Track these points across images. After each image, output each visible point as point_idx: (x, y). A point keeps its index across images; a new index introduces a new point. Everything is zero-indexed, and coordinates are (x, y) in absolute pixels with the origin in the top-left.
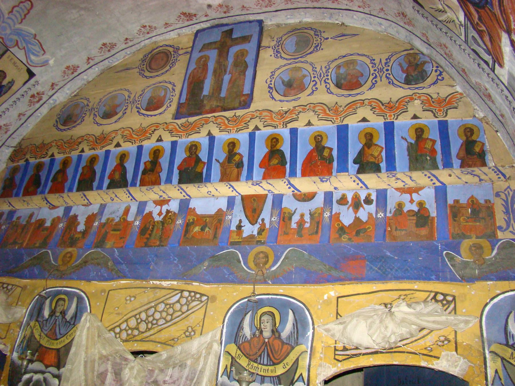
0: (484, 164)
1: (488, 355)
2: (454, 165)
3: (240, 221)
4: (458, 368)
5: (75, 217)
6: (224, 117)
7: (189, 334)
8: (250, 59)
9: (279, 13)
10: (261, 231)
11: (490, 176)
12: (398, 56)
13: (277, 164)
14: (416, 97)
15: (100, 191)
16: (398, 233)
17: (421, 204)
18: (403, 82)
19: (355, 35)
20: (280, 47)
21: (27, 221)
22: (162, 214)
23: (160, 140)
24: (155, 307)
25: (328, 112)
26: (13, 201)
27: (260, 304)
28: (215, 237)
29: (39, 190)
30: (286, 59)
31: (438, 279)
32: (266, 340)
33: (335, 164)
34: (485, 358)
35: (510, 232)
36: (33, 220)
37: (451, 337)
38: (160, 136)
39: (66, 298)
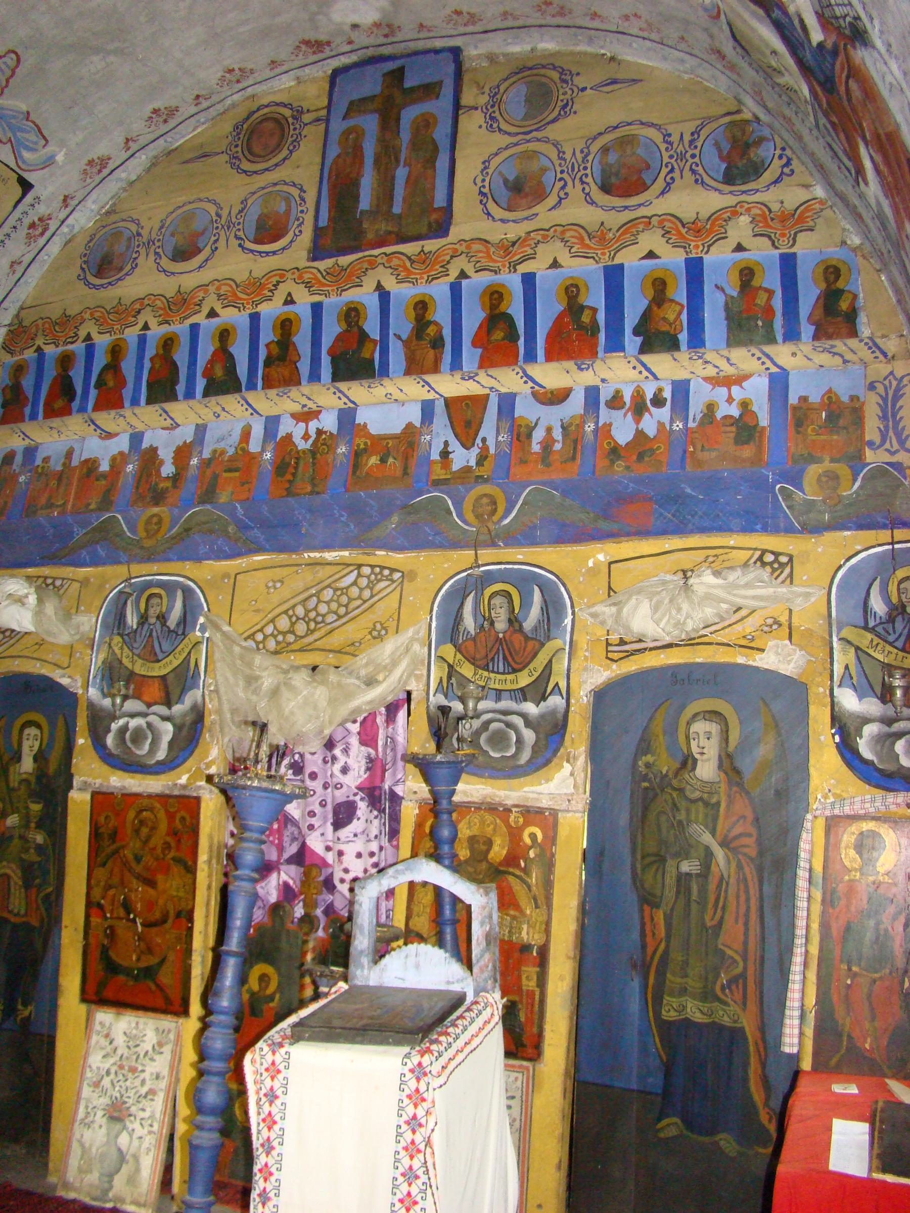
0: (853, 333)
1: (835, 645)
2: (803, 335)
3: (446, 443)
4: (792, 665)
5: (153, 450)
6: (402, 254)
7: (378, 634)
8: (441, 133)
9: (490, 35)
10: (482, 459)
11: (860, 354)
12: (714, 125)
13: (503, 339)
14: (743, 210)
15: (192, 402)
16: (705, 456)
17: (745, 405)
18: (721, 179)
19: (635, 81)
20: (496, 107)
21: (64, 464)
22: (310, 437)
23: (289, 301)
24: (317, 594)
25: (587, 241)
26: (28, 427)
27: (487, 579)
28: (405, 473)
29: (75, 405)
30: (509, 134)
31: (765, 529)
32: (501, 635)
33: (602, 336)
34: (831, 649)
35: (887, 450)
36: (75, 462)
37: (784, 619)
38: (289, 294)
39: (163, 592)
